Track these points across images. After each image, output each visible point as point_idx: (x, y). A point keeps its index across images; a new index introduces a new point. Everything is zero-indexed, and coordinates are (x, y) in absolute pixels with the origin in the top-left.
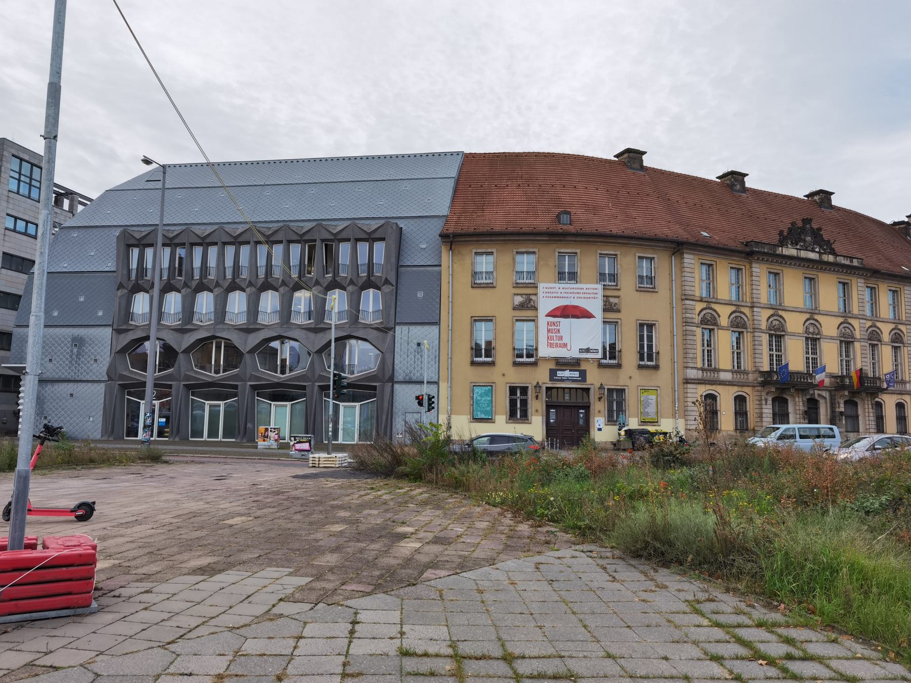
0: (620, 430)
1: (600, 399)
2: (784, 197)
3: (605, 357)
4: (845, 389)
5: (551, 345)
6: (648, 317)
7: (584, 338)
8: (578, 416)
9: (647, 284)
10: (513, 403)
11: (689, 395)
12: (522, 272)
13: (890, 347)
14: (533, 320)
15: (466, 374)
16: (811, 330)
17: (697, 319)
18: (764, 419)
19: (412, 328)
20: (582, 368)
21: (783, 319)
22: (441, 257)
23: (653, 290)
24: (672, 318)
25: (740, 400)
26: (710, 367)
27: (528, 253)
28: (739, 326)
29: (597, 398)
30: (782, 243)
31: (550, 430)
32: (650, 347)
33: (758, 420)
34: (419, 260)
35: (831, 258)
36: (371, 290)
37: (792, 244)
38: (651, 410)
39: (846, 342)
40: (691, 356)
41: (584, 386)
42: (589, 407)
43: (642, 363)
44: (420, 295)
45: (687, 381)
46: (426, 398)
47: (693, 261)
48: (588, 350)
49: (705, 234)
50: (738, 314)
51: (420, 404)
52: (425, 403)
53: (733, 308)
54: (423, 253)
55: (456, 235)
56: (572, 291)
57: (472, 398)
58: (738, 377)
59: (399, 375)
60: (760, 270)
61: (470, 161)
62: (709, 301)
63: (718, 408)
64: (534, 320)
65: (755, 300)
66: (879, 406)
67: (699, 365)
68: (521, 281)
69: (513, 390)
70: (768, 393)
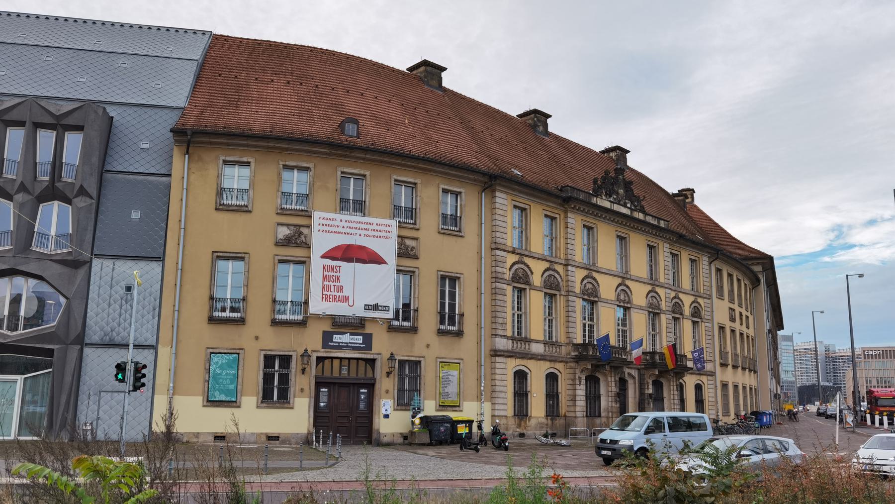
0: (413, 417)
1: (388, 374)
4: (655, 368)
5: (326, 298)
6: (452, 268)
7: (371, 289)
10: (268, 379)
12: (290, 194)
13: (690, 322)
14: (304, 262)
15: (200, 335)
16: (622, 297)
17: (508, 275)
19: (119, 263)
20: (368, 330)
21: (597, 282)
22: (172, 156)
23: (458, 234)
24: (479, 271)
25: (552, 379)
26: (520, 338)
27: (301, 169)
28: (552, 288)
29: (384, 373)
30: (597, 194)
31: (320, 418)
32: (452, 307)
33: (571, 403)
34: (137, 165)
35: (641, 216)
36: (56, 204)
37: (606, 195)
38: (452, 389)
39: (654, 313)
40: (500, 320)
41: (369, 356)
42: (373, 385)
43: (442, 327)
44: (136, 215)
45: (496, 353)
46: (130, 367)
47: (505, 202)
48: (375, 307)
49: (517, 172)
50: (551, 272)
53: (547, 265)
54: (144, 155)
55: (196, 133)
56: (358, 225)
57: (208, 371)
59: (94, 334)
60: (575, 221)
61: (220, 45)
62: (522, 253)
63: (529, 389)
64: (304, 263)
66: (681, 388)
69: (269, 360)
70: (582, 371)
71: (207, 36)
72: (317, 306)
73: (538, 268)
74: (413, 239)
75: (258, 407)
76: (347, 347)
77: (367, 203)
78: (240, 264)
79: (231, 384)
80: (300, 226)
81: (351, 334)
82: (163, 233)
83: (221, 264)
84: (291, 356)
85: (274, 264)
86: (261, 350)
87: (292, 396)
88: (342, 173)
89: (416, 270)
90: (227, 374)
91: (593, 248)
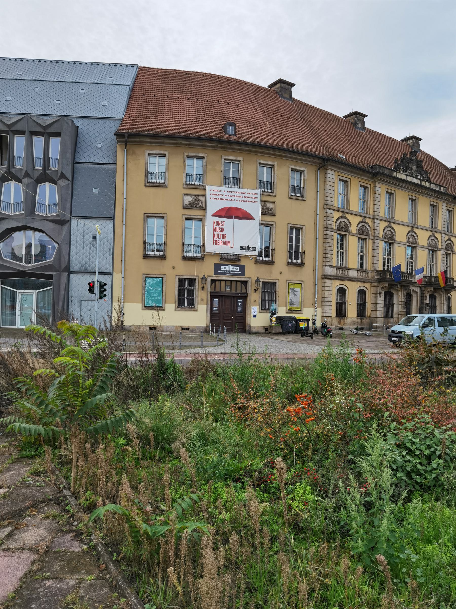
0: (272, 317)
1: (256, 290)
2: (389, 138)
3: (261, 255)
5: (216, 242)
6: (297, 222)
7: (244, 236)
8: (237, 305)
9: (297, 192)
10: (181, 293)
11: (326, 288)
16: (411, 240)
17: (335, 226)
18: (378, 309)
19: (88, 222)
20: (242, 263)
21: (394, 230)
23: (302, 199)
24: (316, 224)
25: (362, 293)
26: (342, 267)
31: (213, 317)
32: (297, 247)
35: (427, 184)
36: (47, 184)
38: (296, 300)
39: (433, 250)
41: (243, 279)
43: (291, 261)
44: (96, 191)
45: (325, 277)
46: (97, 285)
47: (334, 177)
48: (247, 248)
50: (363, 224)
51: (91, 290)
52: (97, 290)
54: (99, 151)
55: (131, 135)
56: (235, 194)
57: (144, 288)
58: (362, 275)
60: (381, 189)
61: (143, 72)
62: (344, 211)
63: (346, 300)
64: (201, 220)
65: (376, 213)
68: (191, 183)
69: (181, 281)
72: (210, 248)
73: (354, 221)
75: (175, 310)
76: (230, 273)
78: (162, 221)
79: (159, 296)
80: (198, 196)
81: (232, 265)
82: (113, 202)
88: (225, 159)
89: (274, 223)
90: (156, 290)
91: (393, 207)
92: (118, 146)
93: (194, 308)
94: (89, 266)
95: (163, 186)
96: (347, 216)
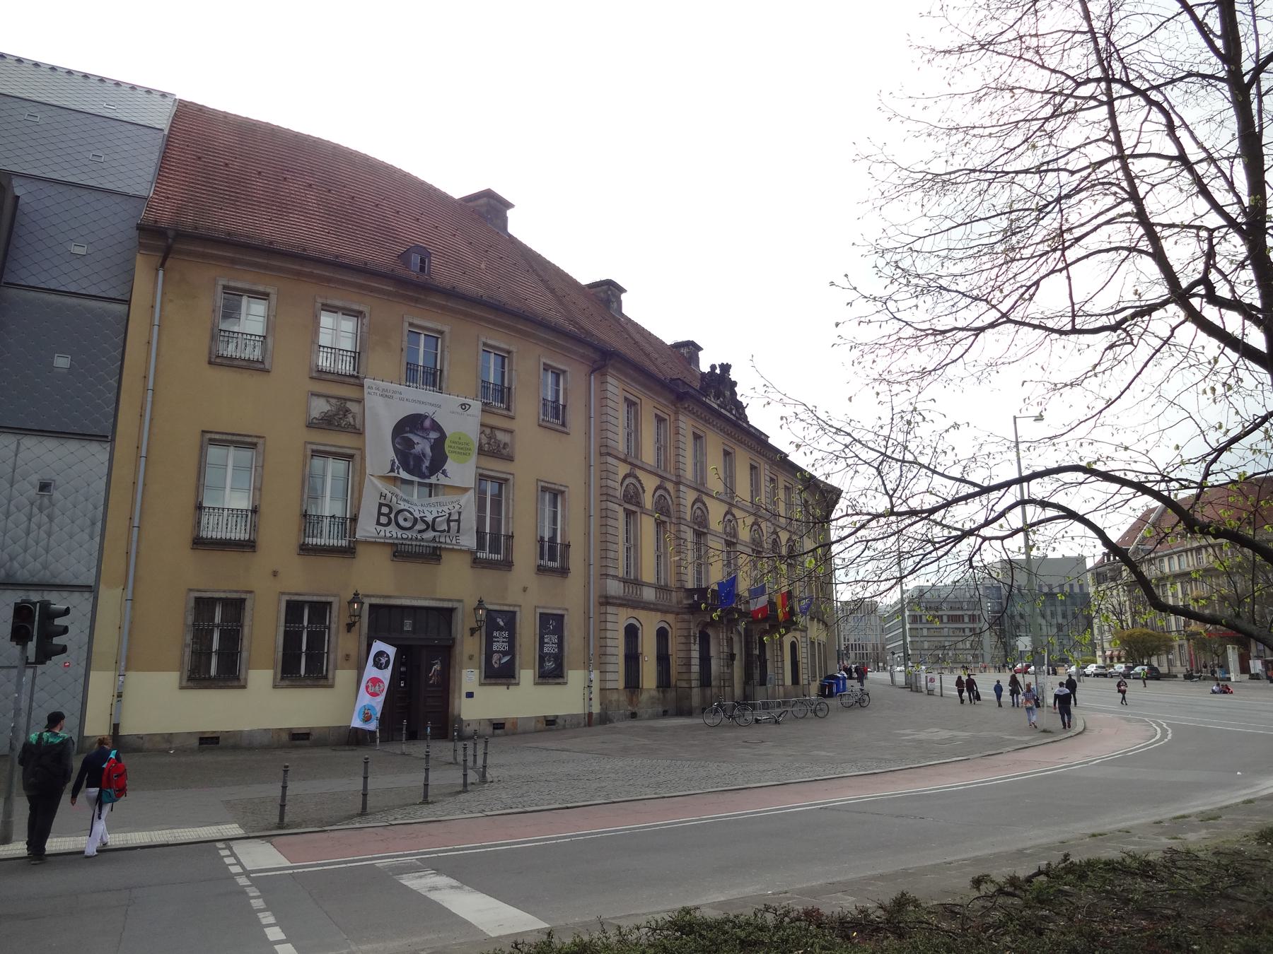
10: (291, 640)
17: (619, 493)
19: (28, 442)
25: (662, 634)
27: (348, 312)
55: (182, 236)
67: (621, 573)
69: (294, 609)
71: (169, 101)
73: (650, 483)
74: (506, 431)
75: (275, 687)
77: (445, 373)
78: (246, 455)
80: (346, 400)
82: (112, 396)
83: (214, 453)
84: (330, 603)
85: (305, 456)
86: (283, 593)
87: (243, 667)
88: (411, 324)
91: (702, 463)
92: (139, 257)
93: (238, 679)
94: (23, 567)
95: (256, 367)
96: (639, 473)
